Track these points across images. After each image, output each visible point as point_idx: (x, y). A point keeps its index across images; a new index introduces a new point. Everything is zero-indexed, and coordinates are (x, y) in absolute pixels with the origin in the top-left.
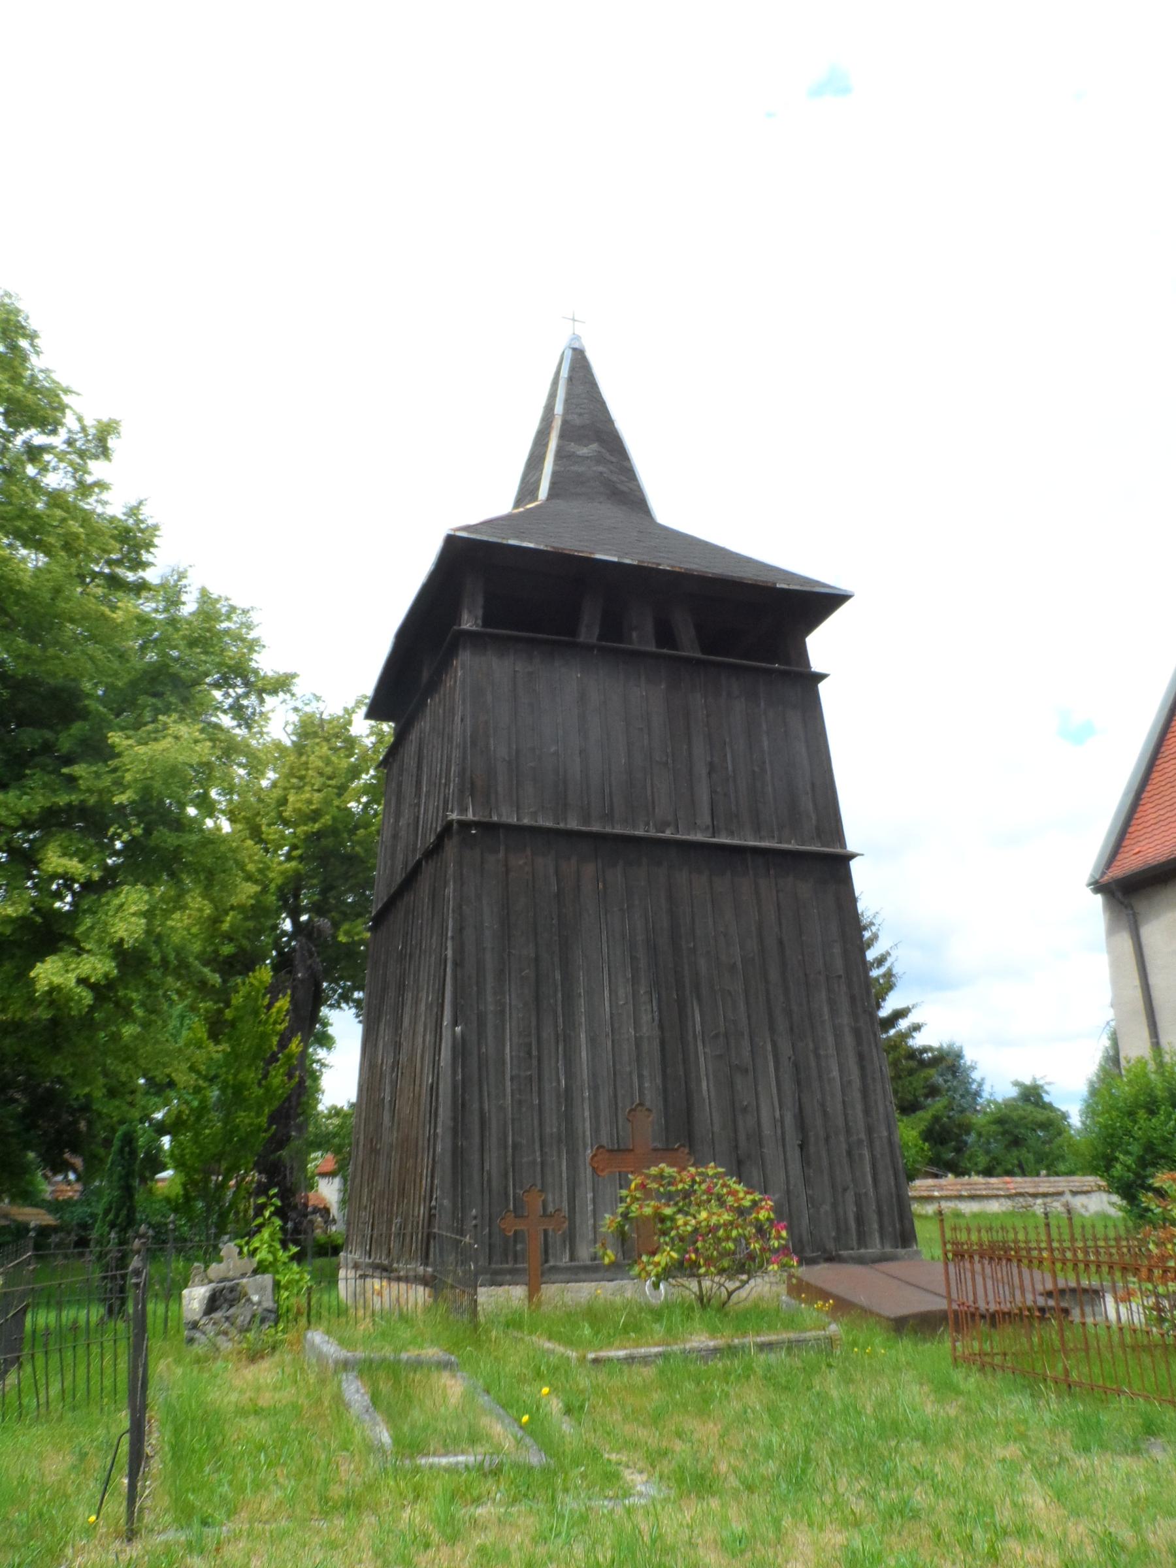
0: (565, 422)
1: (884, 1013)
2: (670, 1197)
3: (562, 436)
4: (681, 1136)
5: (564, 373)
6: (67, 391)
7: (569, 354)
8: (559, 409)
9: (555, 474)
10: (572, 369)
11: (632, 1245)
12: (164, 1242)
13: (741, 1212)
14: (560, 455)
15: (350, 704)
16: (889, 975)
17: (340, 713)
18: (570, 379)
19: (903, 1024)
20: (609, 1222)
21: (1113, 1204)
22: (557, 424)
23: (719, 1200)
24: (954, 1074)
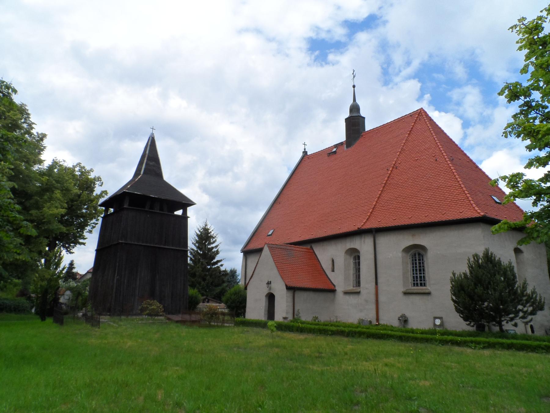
0: (148, 156)
1: (215, 261)
2: (149, 304)
3: (147, 159)
4: (152, 295)
5: (149, 144)
6: (33, 123)
7: (151, 138)
8: (147, 152)
9: (145, 169)
10: (151, 142)
11: (142, 310)
12: (531, 33)
13: (158, 307)
14: (146, 164)
15: (75, 164)
16: (217, 251)
17: (71, 167)
18: (150, 145)
19: (219, 264)
20: (140, 307)
21: (63, 269)
22: (147, 156)
23: (156, 305)
24: (233, 277)
